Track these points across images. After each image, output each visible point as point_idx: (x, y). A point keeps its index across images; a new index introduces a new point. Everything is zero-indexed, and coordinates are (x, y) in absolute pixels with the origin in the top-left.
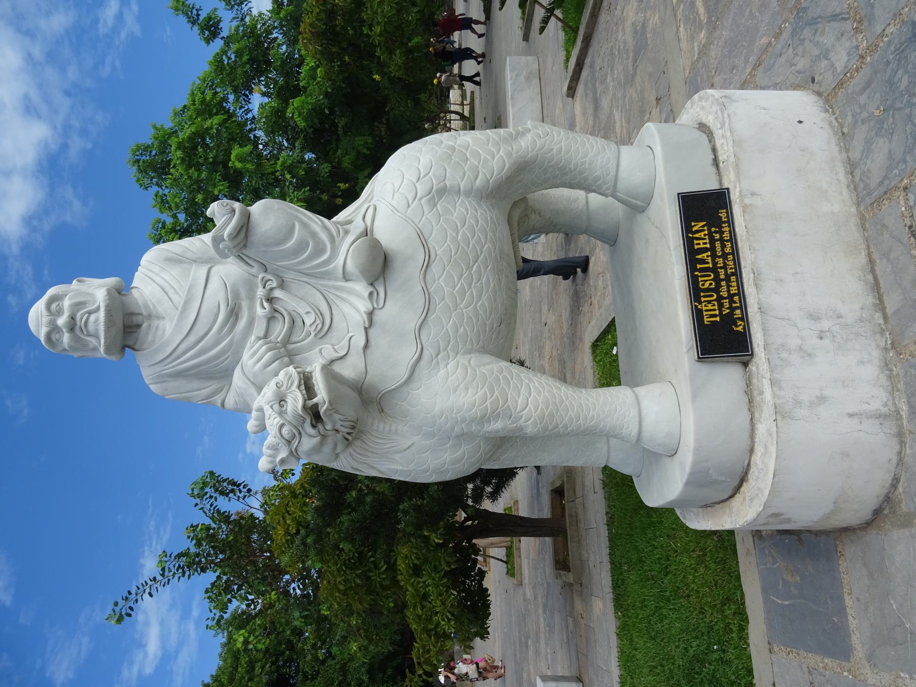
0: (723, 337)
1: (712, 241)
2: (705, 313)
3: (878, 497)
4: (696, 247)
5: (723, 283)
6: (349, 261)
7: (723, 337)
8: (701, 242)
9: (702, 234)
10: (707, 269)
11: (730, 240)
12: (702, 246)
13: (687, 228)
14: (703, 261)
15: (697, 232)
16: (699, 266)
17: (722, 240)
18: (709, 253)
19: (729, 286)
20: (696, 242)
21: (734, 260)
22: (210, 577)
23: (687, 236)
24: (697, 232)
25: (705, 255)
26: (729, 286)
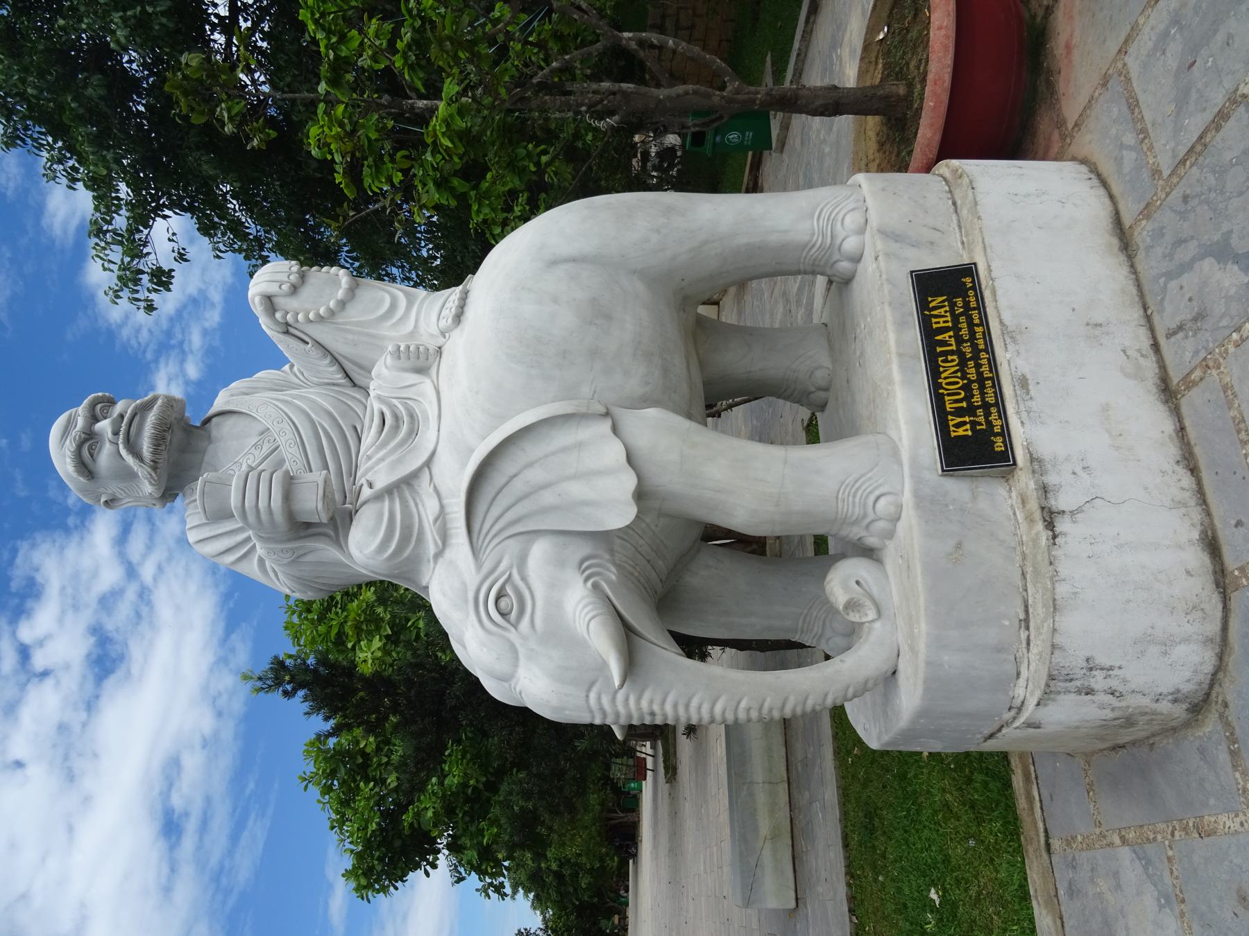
0: (973, 442)
1: (955, 319)
2: (947, 398)
3: (1068, 47)
4: (935, 326)
5: (962, 319)
6: (414, 510)
7: (973, 442)
8: (941, 320)
9: (942, 310)
10: (952, 353)
11: (996, 404)
12: (942, 325)
13: (923, 305)
14: (944, 343)
15: (935, 308)
16: (939, 349)
17: (981, 380)
18: (951, 333)
19: (983, 394)
20: (934, 320)
21: (976, 295)
22: (176, 816)
23: (923, 315)
24: (935, 308)
25: (946, 335)
26: (983, 394)
